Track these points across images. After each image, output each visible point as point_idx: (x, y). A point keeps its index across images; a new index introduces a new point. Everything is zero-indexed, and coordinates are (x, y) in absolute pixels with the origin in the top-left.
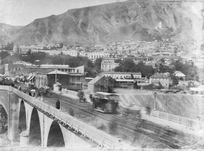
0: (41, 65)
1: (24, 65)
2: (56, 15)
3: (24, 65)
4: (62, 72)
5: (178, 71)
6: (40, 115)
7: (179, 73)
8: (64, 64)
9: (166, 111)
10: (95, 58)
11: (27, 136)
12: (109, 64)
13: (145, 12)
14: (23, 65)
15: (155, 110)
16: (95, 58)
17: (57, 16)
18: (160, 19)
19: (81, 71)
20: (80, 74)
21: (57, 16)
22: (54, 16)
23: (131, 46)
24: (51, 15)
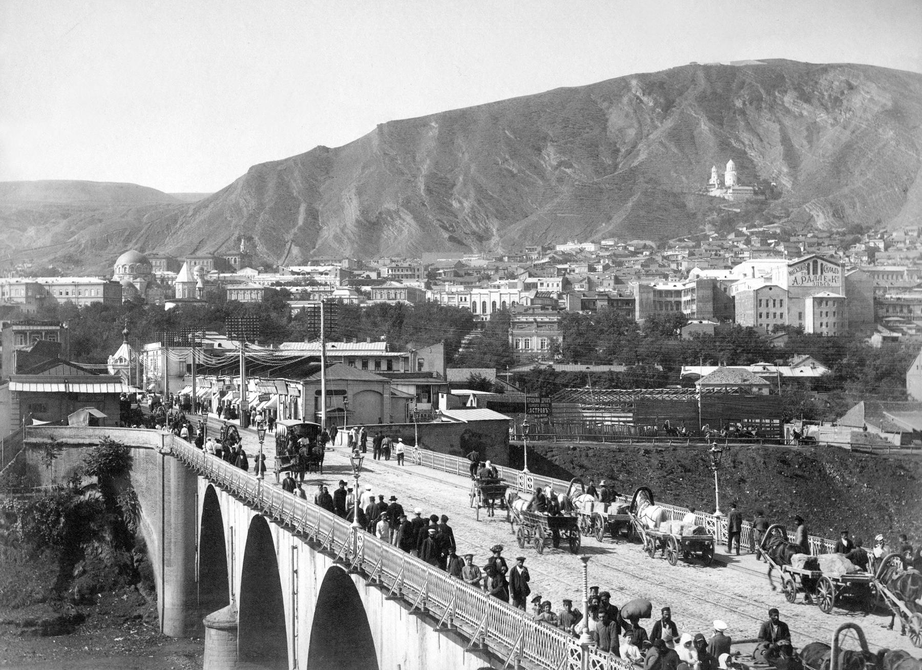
0: (281, 347)
1: (216, 346)
2: (332, 145)
3: (216, 346)
4: (576, 366)
5: (804, 357)
6: (282, 540)
7: (807, 362)
8: (368, 339)
9: (860, 247)
10: (484, 310)
11: (231, 629)
12: (538, 336)
13: (669, 123)
14: (212, 345)
15: (718, 518)
16: (484, 310)
17: (337, 150)
18: (726, 149)
19: (431, 364)
20: (430, 375)
21: (335, 149)
22: (325, 149)
23: (623, 259)
24: (315, 146)
